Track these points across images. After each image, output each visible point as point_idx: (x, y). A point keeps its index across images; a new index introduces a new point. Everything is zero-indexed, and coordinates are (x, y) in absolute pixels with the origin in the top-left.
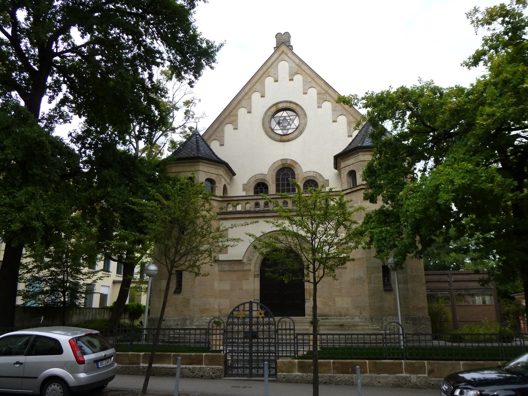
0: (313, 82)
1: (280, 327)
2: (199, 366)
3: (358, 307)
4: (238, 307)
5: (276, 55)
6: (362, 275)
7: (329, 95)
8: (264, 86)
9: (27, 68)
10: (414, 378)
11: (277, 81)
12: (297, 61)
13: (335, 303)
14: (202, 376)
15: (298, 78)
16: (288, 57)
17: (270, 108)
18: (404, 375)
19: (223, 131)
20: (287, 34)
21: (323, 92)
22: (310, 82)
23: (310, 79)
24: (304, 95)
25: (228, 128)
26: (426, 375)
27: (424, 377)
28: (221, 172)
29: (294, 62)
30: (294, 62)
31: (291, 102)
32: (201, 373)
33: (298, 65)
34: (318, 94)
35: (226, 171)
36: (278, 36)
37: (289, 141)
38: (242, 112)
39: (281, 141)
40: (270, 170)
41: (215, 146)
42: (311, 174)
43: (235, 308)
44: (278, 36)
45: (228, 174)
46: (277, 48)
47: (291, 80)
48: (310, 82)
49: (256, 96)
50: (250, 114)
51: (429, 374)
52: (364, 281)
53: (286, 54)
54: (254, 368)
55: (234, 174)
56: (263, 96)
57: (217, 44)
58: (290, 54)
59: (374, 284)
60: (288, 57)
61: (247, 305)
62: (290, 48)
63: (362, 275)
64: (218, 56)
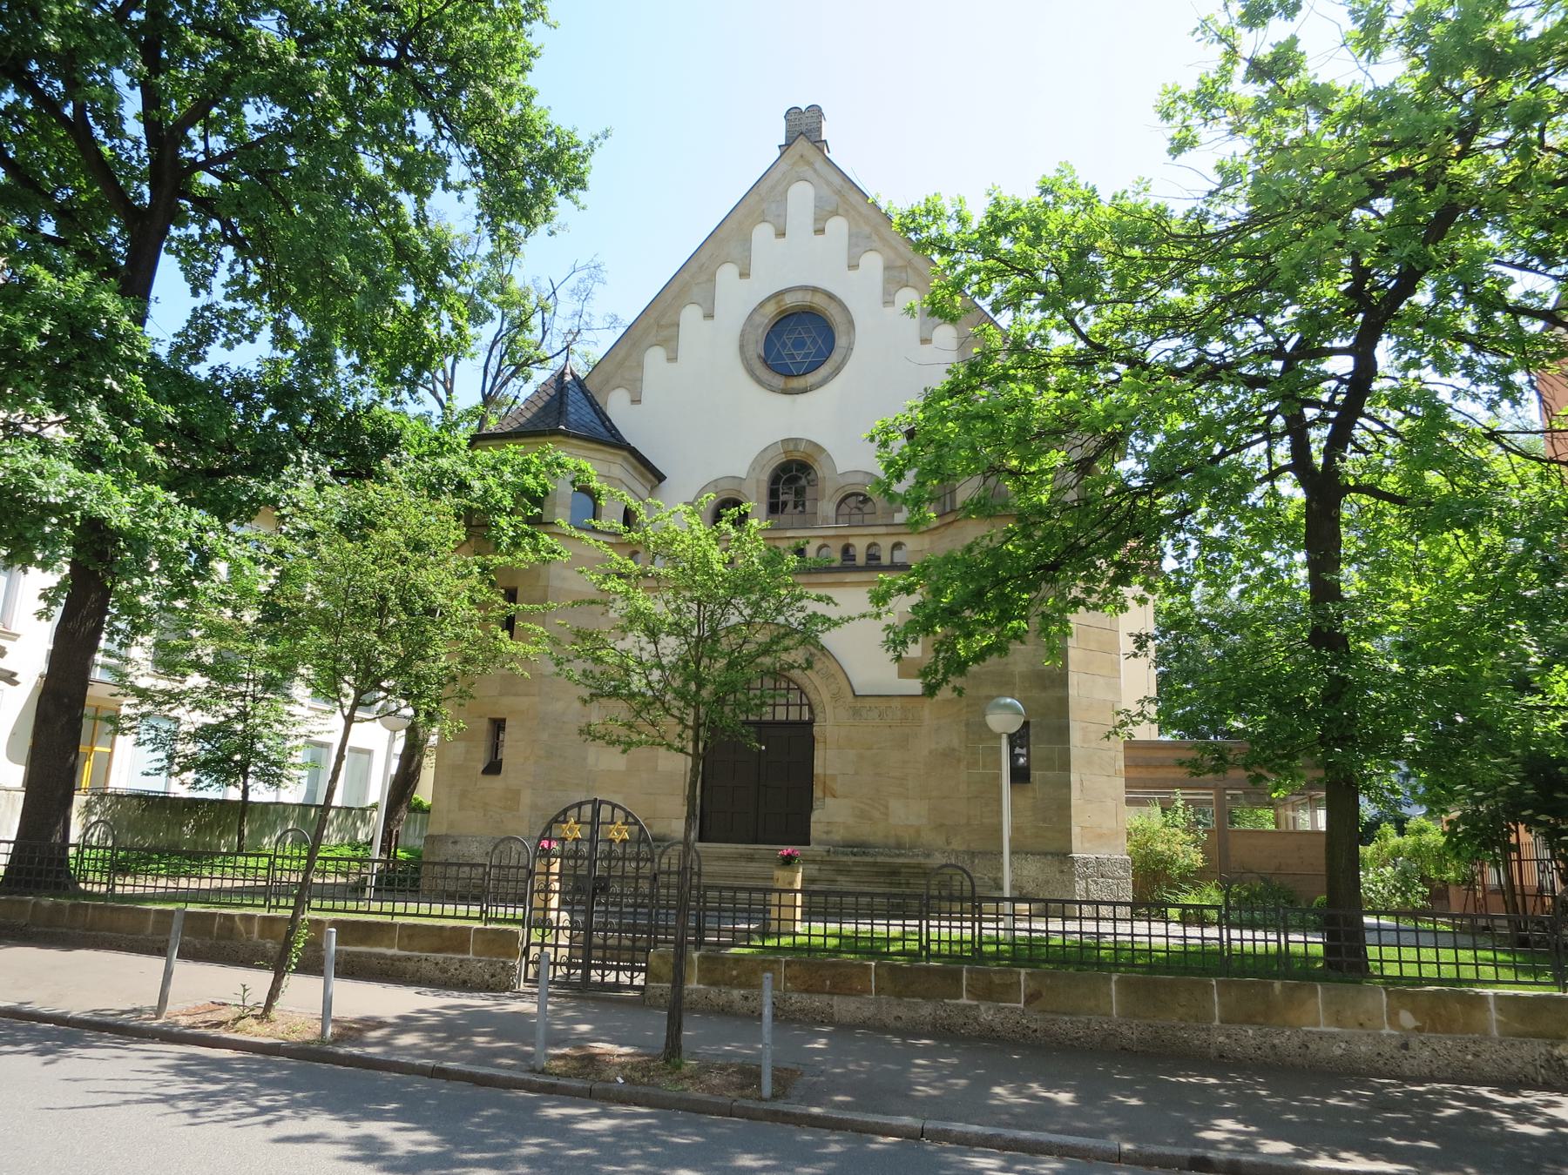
0: (875, 237)
1: (664, 867)
2: (460, 956)
3: (942, 825)
4: (565, 811)
5: (783, 166)
6: (956, 743)
7: (915, 269)
8: (750, 249)
9: (120, 201)
10: (987, 1013)
11: (784, 235)
12: (837, 180)
13: (887, 814)
14: (465, 982)
15: (838, 227)
16: (815, 170)
17: (762, 305)
18: (964, 1001)
19: (640, 366)
20: (816, 112)
21: (899, 263)
22: (869, 237)
23: (867, 230)
24: (852, 273)
25: (654, 357)
26: (1021, 1005)
27: (1013, 1010)
28: (618, 466)
29: (829, 183)
30: (829, 183)
31: (815, 290)
32: (464, 975)
33: (839, 192)
34: (887, 268)
35: (635, 468)
36: (793, 115)
37: (804, 391)
38: (690, 316)
39: (786, 392)
40: (753, 468)
41: (617, 406)
42: (859, 479)
43: (558, 815)
44: (793, 115)
45: (642, 475)
46: (785, 148)
47: (820, 231)
48: (869, 237)
49: (727, 275)
50: (709, 322)
51: (1027, 1002)
52: (959, 761)
53: (810, 164)
54: (596, 967)
55: (660, 477)
56: (744, 274)
57: (583, 137)
58: (819, 164)
59: (984, 767)
60: (815, 170)
61: (587, 810)
62: (819, 144)
63: (956, 743)
64: (597, 171)
